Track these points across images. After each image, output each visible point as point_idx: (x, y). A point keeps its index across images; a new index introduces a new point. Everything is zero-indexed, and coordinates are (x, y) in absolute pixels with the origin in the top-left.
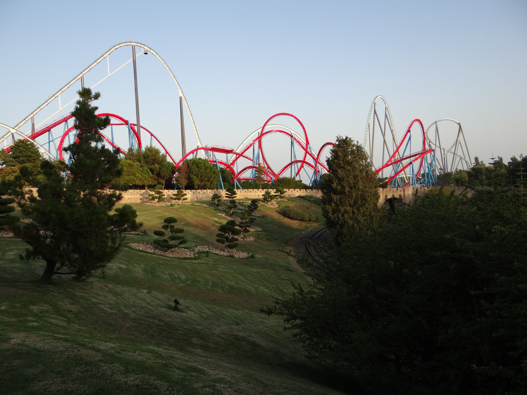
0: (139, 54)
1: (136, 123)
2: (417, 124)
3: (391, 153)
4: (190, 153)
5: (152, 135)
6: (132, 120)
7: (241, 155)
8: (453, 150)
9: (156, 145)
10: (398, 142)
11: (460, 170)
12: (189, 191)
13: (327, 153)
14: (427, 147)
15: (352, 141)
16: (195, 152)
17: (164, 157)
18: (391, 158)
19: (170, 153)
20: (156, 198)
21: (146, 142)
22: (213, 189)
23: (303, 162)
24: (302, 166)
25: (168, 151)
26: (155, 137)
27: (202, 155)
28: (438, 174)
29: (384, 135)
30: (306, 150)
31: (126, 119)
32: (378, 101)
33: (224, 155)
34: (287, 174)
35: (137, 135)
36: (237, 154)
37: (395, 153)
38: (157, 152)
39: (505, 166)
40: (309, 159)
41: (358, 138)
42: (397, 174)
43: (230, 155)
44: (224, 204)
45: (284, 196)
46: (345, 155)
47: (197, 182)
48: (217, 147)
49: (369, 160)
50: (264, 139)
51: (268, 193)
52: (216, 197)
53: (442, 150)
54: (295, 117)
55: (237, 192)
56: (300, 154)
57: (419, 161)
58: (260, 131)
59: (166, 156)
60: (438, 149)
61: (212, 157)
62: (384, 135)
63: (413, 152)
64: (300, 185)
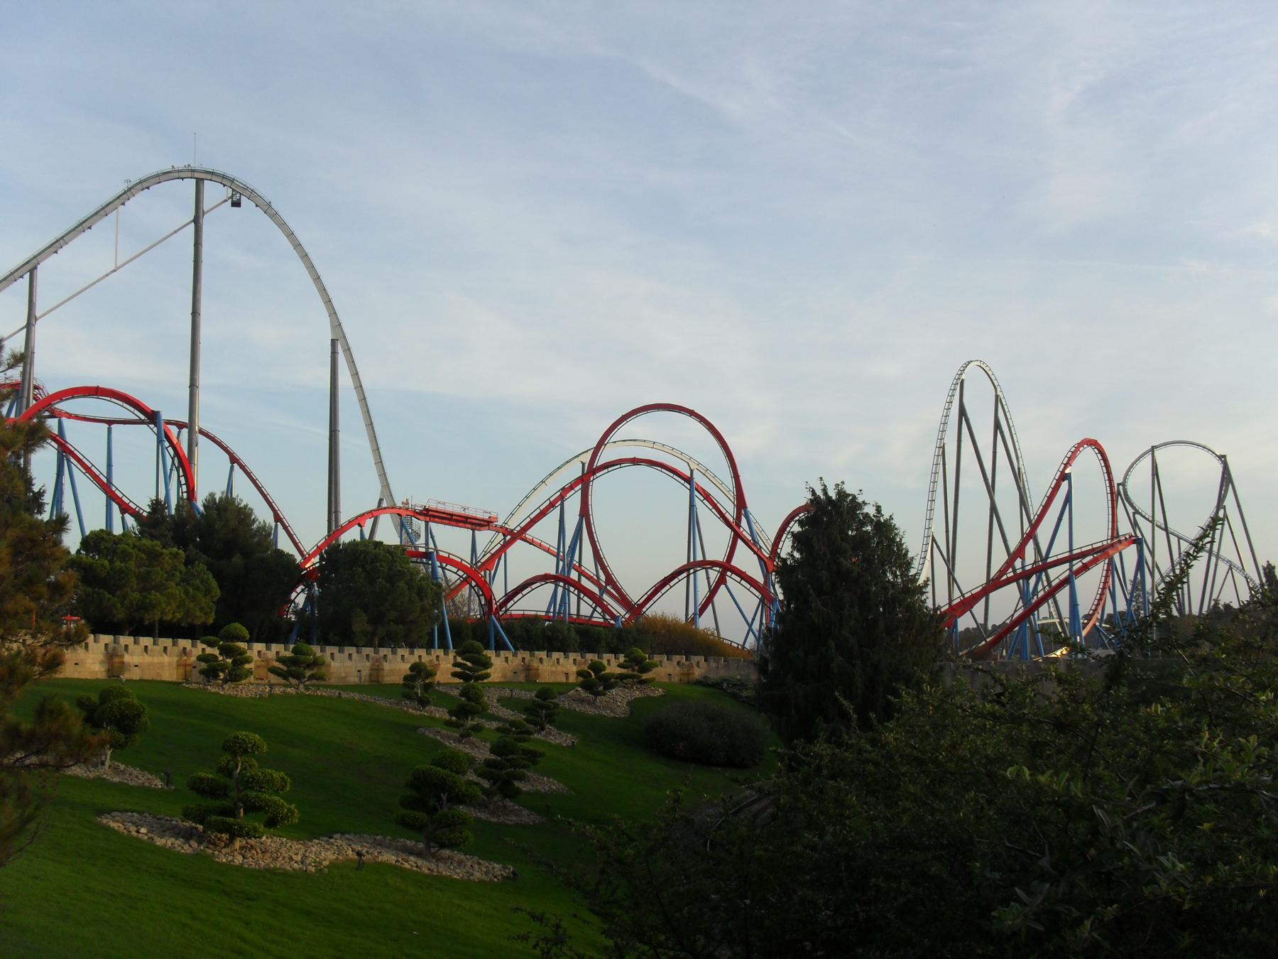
0: (215, 193)
1: (186, 420)
2: (1088, 453)
3: (1014, 544)
4: (350, 524)
5: (234, 460)
6: (174, 410)
9: (245, 494)
10: (1035, 508)
11: (1227, 606)
12: (335, 650)
14: (1125, 528)
15: (860, 506)
16: (369, 523)
18: (1009, 564)
19: (289, 520)
20: (223, 668)
21: (211, 480)
22: (412, 646)
23: (726, 567)
26: (243, 467)
27: (388, 534)
29: (991, 489)
30: (734, 527)
31: (152, 406)
32: (973, 377)
33: (466, 533)
34: (671, 606)
35: (185, 464)
36: (506, 532)
38: (244, 515)
39: (955, 626)
40: (746, 560)
41: (896, 490)
42: (1031, 609)
44: (443, 698)
45: (653, 679)
46: (838, 551)
47: (360, 623)
48: (440, 507)
49: (913, 572)
50: (599, 485)
51: (597, 667)
52: (418, 671)
53: (1174, 539)
54: (702, 420)
56: (716, 541)
57: (1098, 571)
58: (587, 458)
60: (1160, 534)
61: (422, 541)
62: (991, 489)
63: (1081, 543)
64: (710, 647)
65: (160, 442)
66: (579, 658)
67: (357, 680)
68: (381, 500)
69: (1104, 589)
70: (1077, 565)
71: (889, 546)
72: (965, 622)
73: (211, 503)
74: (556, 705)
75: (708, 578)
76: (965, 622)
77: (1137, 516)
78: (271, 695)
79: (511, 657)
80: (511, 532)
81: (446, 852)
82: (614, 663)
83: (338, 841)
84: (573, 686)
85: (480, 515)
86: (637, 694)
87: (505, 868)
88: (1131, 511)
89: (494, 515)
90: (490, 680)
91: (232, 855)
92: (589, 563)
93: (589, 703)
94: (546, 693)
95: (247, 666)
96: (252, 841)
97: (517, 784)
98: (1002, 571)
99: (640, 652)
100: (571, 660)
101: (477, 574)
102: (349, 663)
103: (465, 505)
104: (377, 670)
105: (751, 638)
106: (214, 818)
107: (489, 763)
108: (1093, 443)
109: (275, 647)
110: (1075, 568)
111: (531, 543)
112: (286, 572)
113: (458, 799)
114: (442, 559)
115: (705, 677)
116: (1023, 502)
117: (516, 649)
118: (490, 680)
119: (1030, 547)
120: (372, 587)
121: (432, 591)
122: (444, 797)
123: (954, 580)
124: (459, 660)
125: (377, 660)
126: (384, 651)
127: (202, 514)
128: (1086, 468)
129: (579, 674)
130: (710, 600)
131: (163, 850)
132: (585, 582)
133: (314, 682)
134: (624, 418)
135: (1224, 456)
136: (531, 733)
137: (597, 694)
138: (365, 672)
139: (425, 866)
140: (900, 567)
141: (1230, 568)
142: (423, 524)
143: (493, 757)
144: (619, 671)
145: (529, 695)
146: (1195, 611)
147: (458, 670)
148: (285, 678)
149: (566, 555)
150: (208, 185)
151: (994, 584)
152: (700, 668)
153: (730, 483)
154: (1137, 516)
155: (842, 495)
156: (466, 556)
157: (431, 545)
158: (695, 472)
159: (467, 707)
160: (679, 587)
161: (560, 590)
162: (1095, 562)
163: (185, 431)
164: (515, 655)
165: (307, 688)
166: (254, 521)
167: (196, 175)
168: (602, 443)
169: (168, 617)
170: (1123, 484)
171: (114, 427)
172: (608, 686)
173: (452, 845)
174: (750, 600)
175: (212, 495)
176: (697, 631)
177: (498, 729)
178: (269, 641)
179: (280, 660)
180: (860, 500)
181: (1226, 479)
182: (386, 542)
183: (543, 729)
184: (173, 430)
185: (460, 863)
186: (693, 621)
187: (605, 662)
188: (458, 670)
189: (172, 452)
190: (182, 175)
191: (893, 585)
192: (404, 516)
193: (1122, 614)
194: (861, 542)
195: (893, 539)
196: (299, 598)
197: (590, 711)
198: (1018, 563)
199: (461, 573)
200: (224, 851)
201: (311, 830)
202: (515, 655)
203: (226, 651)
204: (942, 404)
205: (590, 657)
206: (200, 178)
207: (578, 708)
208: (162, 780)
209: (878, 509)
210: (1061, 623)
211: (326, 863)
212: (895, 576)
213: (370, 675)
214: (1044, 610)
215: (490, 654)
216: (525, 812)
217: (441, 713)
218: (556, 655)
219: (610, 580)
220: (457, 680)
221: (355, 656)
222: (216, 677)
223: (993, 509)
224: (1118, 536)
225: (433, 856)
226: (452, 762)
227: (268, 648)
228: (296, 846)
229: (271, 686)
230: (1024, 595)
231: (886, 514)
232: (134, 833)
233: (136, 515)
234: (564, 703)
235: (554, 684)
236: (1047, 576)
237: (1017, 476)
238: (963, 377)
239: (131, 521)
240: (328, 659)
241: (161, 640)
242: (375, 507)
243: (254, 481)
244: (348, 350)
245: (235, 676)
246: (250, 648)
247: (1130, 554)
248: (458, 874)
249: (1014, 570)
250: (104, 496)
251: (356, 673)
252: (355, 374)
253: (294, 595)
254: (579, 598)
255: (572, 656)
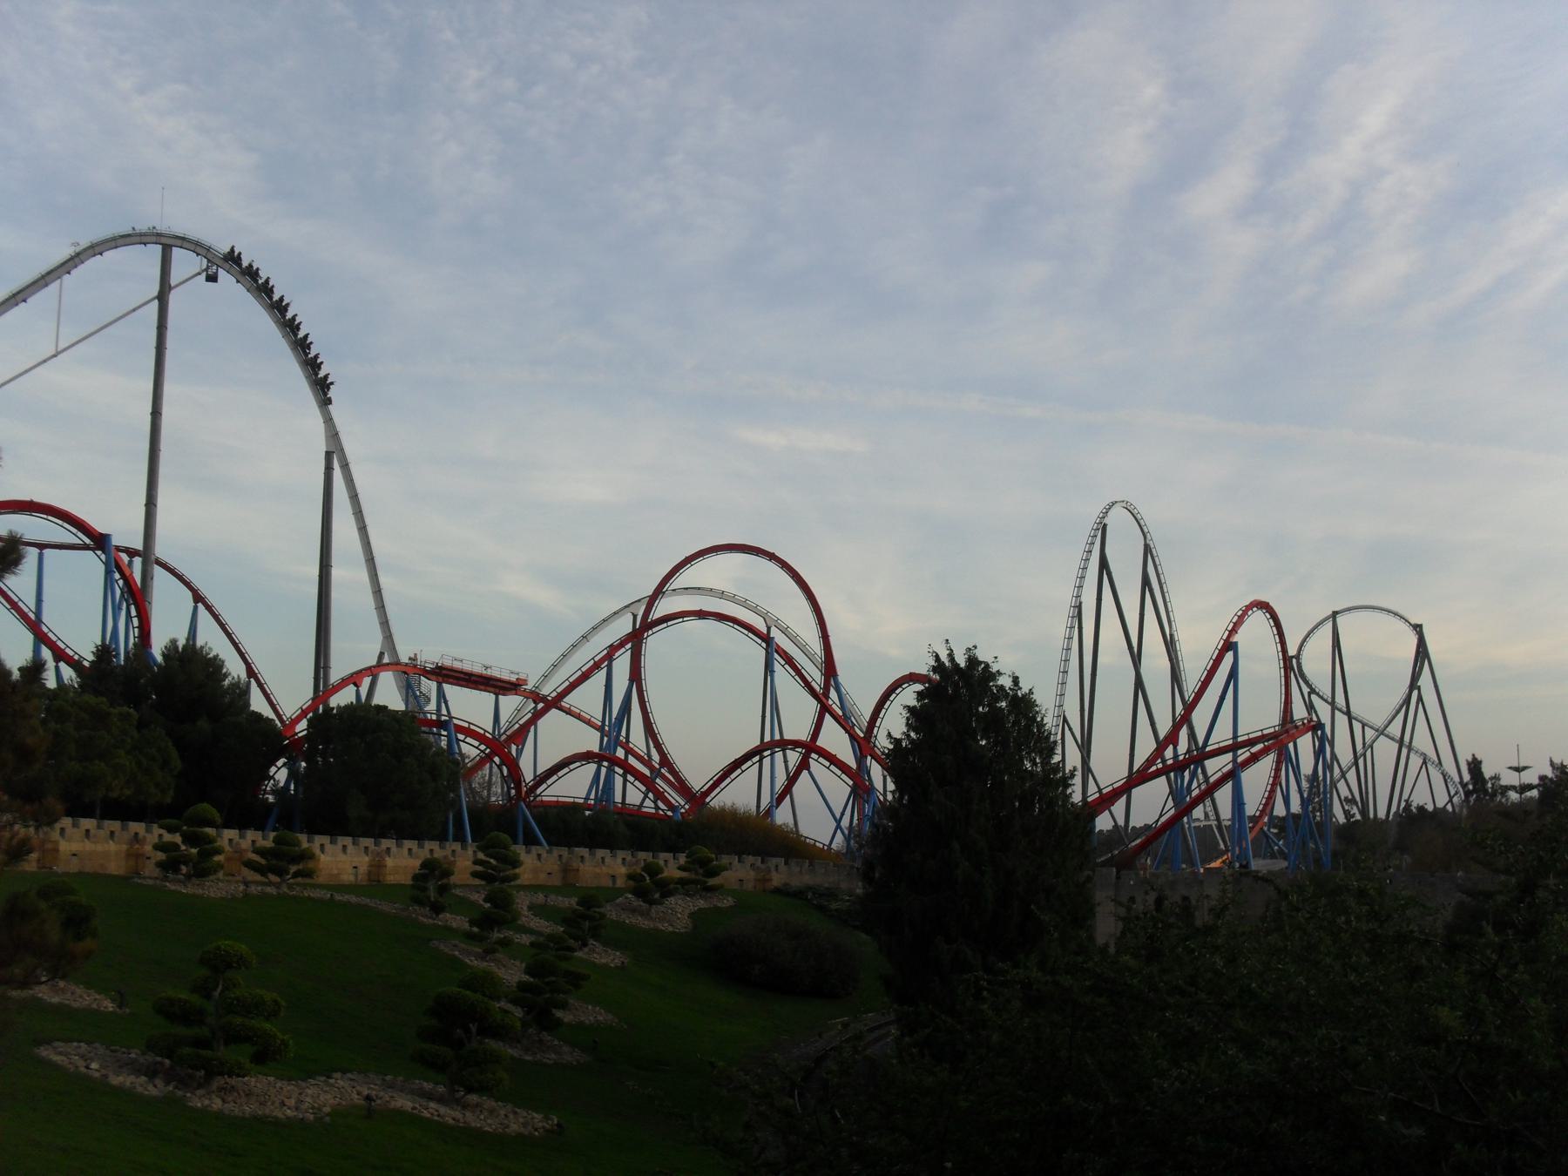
0: (185, 263)
1: (139, 546)
2: (1258, 619)
3: (1164, 728)
4: (344, 682)
5: (198, 598)
6: (125, 529)
7: (555, 703)
8: (1395, 730)
9: (211, 640)
10: (1191, 685)
11: (1421, 809)
12: (325, 839)
13: (894, 723)
14: (1299, 712)
15: (993, 676)
16: (367, 681)
17: (240, 693)
18: (1161, 747)
20: (186, 860)
21: (169, 625)
22: (419, 837)
23: (810, 747)
24: (804, 765)
25: (260, 666)
26: (209, 608)
27: (388, 694)
28: (1341, 819)
29: (1136, 658)
30: (821, 698)
31: (101, 528)
32: (1118, 520)
33: (486, 699)
34: (740, 795)
35: (138, 597)
36: (535, 696)
37: (1176, 728)
38: (214, 667)
40: (834, 739)
41: (1026, 658)
42: (1184, 810)
43: (510, 703)
45: (722, 886)
48: (457, 665)
49: (1057, 759)
50: (655, 643)
51: (653, 870)
52: (432, 871)
53: (1357, 726)
54: (784, 565)
55: (523, 856)
56: (798, 715)
57: (1268, 762)
59: (246, 692)
60: (1341, 720)
61: (432, 706)
62: (1136, 658)
63: (1247, 728)
64: (791, 846)
65: (108, 573)
66: (629, 858)
67: (352, 878)
68: (381, 655)
69: (1274, 785)
70: (1243, 754)
71: (1028, 727)
72: (1103, 823)
73: (171, 651)
74: (603, 916)
75: (786, 762)
76: (1103, 823)
77: (1313, 697)
78: (246, 895)
79: (544, 855)
80: (543, 699)
81: (473, 1098)
82: (672, 864)
83: (340, 1081)
84: (620, 892)
85: (505, 676)
86: (702, 904)
87: (547, 1118)
88: (1306, 690)
89: (522, 676)
90: (518, 882)
91: (197, 1101)
92: (638, 738)
93: (642, 914)
94: (590, 900)
95: (217, 858)
96: (234, 1081)
97: (559, 1014)
98: (1150, 761)
99: (706, 852)
100: (619, 861)
101: (502, 746)
102: (342, 857)
103: (488, 663)
104: (377, 866)
105: (839, 837)
106: (187, 1050)
107: (522, 986)
108: (1264, 606)
109: (251, 835)
110: (1240, 760)
111: (568, 712)
112: (267, 739)
113: (497, 1031)
114: (460, 729)
115: (786, 884)
116: (1176, 677)
117: (549, 844)
118: (518, 882)
119: (1183, 734)
120: (378, 760)
121: (451, 769)
122: (473, 1028)
123: (1090, 770)
124: (481, 856)
125: (378, 854)
126: (386, 843)
127: (159, 666)
128: (1256, 637)
129: (630, 877)
130: (788, 790)
131: (119, 1091)
132: (632, 761)
133: (300, 879)
134: (689, 560)
135: (1420, 626)
136: (573, 950)
137: (651, 903)
138: (363, 869)
139: (449, 1114)
140: (1041, 753)
141: (1425, 762)
142: (434, 685)
143: (526, 978)
144: (679, 874)
145: (570, 902)
146: (1382, 814)
147: (479, 868)
148: (263, 874)
149: (612, 728)
150: (177, 253)
151: (1138, 777)
152: (781, 874)
153: (816, 646)
154: (1313, 697)
155: (973, 661)
156: (488, 725)
157: (444, 711)
158: (773, 629)
159: (495, 917)
160: (750, 773)
161: (604, 770)
162: (1265, 752)
163: (138, 561)
164: (549, 852)
165: (290, 887)
166: (226, 675)
167: (164, 240)
168: (659, 592)
169: (115, 794)
170: (1298, 657)
171: (47, 552)
172: (666, 894)
173: (482, 1089)
174: (838, 789)
175: (174, 642)
176: (773, 824)
177: (532, 944)
178: (242, 826)
179: (258, 851)
180: (994, 668)
181: (1422, 653)
182: (392, 707)
183: (585, 945)
184: (125, 557)
185: (492, 1111)
186: (769, 812)
187: (662, 863)
188: (479, 868)
189: (121, 582)
190: (144, 239)
191: (1031, 773)
192: (410, 673)
193: (1296, 817)
194: (994, 722)
195: (1034, 718)
196: (280, 773)
197: (644, 923)
198: (1169, 753)
199: (483, 747)
200: (199, 1092)
201: (306, 1070)
202: (549, 852)
203: (190, 839)
204: (1079, 554)
205: (643, 855)
206: (168, 243)
207: (629, 919)
208: (113, 1001)
209: (1016, 680)
210: (1219, 827)
211: (327, 1109)
212: (1034, 764)
213: (370, 873)
214: (1198, 812)
215: (519, 849)
216: (566, 1049)
217: (459, 922)
218: (600, 853)
219: (665, 761)
220: (477, 882)
221: (350, 848)
222: (177, 870)
223: (1139, 684)
224: (1292, 721)
225: (458, 1101)
226: (484, 984)
227: (242, 836)
228: (289, 1088)
229: (246, 883)
230: (1176, 793)
231: (1025, 687)
232: (83, 1069)
233: (75, 664)
234: (611, 912)
235: (599, 888)
236: (1204, 772)
237: (1170, 644)
238: (1106, 521)
239: (68, 673)
240: (317, 851)
241: (107, 823)
242: (374, 662)
243: (223, 626)
244: (345, 466)
245: (202, 870)
246: (219, 835)
247: (1305, 744)
248: (489, 1125)
249: (1164, 761)
250: (31, 637)
251: (351, 870)
252: (354, 497)
253: (273, 769)
254: (625, 780)
255: (621, 854)
